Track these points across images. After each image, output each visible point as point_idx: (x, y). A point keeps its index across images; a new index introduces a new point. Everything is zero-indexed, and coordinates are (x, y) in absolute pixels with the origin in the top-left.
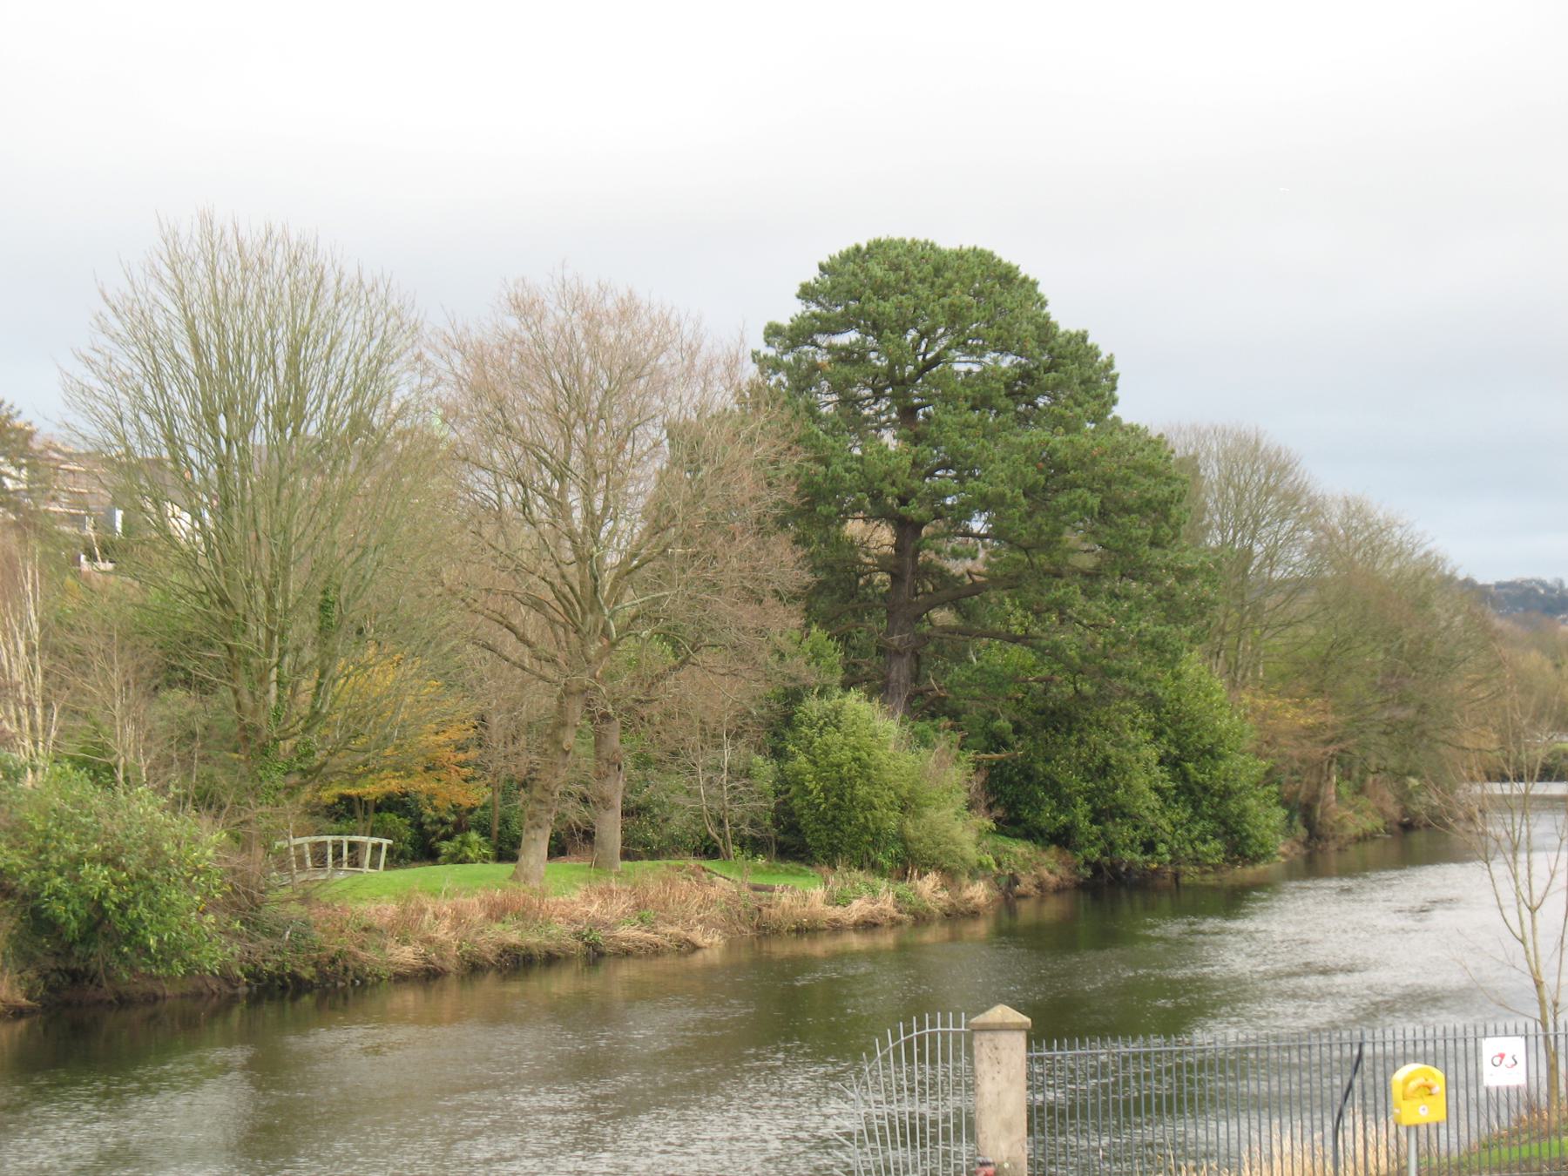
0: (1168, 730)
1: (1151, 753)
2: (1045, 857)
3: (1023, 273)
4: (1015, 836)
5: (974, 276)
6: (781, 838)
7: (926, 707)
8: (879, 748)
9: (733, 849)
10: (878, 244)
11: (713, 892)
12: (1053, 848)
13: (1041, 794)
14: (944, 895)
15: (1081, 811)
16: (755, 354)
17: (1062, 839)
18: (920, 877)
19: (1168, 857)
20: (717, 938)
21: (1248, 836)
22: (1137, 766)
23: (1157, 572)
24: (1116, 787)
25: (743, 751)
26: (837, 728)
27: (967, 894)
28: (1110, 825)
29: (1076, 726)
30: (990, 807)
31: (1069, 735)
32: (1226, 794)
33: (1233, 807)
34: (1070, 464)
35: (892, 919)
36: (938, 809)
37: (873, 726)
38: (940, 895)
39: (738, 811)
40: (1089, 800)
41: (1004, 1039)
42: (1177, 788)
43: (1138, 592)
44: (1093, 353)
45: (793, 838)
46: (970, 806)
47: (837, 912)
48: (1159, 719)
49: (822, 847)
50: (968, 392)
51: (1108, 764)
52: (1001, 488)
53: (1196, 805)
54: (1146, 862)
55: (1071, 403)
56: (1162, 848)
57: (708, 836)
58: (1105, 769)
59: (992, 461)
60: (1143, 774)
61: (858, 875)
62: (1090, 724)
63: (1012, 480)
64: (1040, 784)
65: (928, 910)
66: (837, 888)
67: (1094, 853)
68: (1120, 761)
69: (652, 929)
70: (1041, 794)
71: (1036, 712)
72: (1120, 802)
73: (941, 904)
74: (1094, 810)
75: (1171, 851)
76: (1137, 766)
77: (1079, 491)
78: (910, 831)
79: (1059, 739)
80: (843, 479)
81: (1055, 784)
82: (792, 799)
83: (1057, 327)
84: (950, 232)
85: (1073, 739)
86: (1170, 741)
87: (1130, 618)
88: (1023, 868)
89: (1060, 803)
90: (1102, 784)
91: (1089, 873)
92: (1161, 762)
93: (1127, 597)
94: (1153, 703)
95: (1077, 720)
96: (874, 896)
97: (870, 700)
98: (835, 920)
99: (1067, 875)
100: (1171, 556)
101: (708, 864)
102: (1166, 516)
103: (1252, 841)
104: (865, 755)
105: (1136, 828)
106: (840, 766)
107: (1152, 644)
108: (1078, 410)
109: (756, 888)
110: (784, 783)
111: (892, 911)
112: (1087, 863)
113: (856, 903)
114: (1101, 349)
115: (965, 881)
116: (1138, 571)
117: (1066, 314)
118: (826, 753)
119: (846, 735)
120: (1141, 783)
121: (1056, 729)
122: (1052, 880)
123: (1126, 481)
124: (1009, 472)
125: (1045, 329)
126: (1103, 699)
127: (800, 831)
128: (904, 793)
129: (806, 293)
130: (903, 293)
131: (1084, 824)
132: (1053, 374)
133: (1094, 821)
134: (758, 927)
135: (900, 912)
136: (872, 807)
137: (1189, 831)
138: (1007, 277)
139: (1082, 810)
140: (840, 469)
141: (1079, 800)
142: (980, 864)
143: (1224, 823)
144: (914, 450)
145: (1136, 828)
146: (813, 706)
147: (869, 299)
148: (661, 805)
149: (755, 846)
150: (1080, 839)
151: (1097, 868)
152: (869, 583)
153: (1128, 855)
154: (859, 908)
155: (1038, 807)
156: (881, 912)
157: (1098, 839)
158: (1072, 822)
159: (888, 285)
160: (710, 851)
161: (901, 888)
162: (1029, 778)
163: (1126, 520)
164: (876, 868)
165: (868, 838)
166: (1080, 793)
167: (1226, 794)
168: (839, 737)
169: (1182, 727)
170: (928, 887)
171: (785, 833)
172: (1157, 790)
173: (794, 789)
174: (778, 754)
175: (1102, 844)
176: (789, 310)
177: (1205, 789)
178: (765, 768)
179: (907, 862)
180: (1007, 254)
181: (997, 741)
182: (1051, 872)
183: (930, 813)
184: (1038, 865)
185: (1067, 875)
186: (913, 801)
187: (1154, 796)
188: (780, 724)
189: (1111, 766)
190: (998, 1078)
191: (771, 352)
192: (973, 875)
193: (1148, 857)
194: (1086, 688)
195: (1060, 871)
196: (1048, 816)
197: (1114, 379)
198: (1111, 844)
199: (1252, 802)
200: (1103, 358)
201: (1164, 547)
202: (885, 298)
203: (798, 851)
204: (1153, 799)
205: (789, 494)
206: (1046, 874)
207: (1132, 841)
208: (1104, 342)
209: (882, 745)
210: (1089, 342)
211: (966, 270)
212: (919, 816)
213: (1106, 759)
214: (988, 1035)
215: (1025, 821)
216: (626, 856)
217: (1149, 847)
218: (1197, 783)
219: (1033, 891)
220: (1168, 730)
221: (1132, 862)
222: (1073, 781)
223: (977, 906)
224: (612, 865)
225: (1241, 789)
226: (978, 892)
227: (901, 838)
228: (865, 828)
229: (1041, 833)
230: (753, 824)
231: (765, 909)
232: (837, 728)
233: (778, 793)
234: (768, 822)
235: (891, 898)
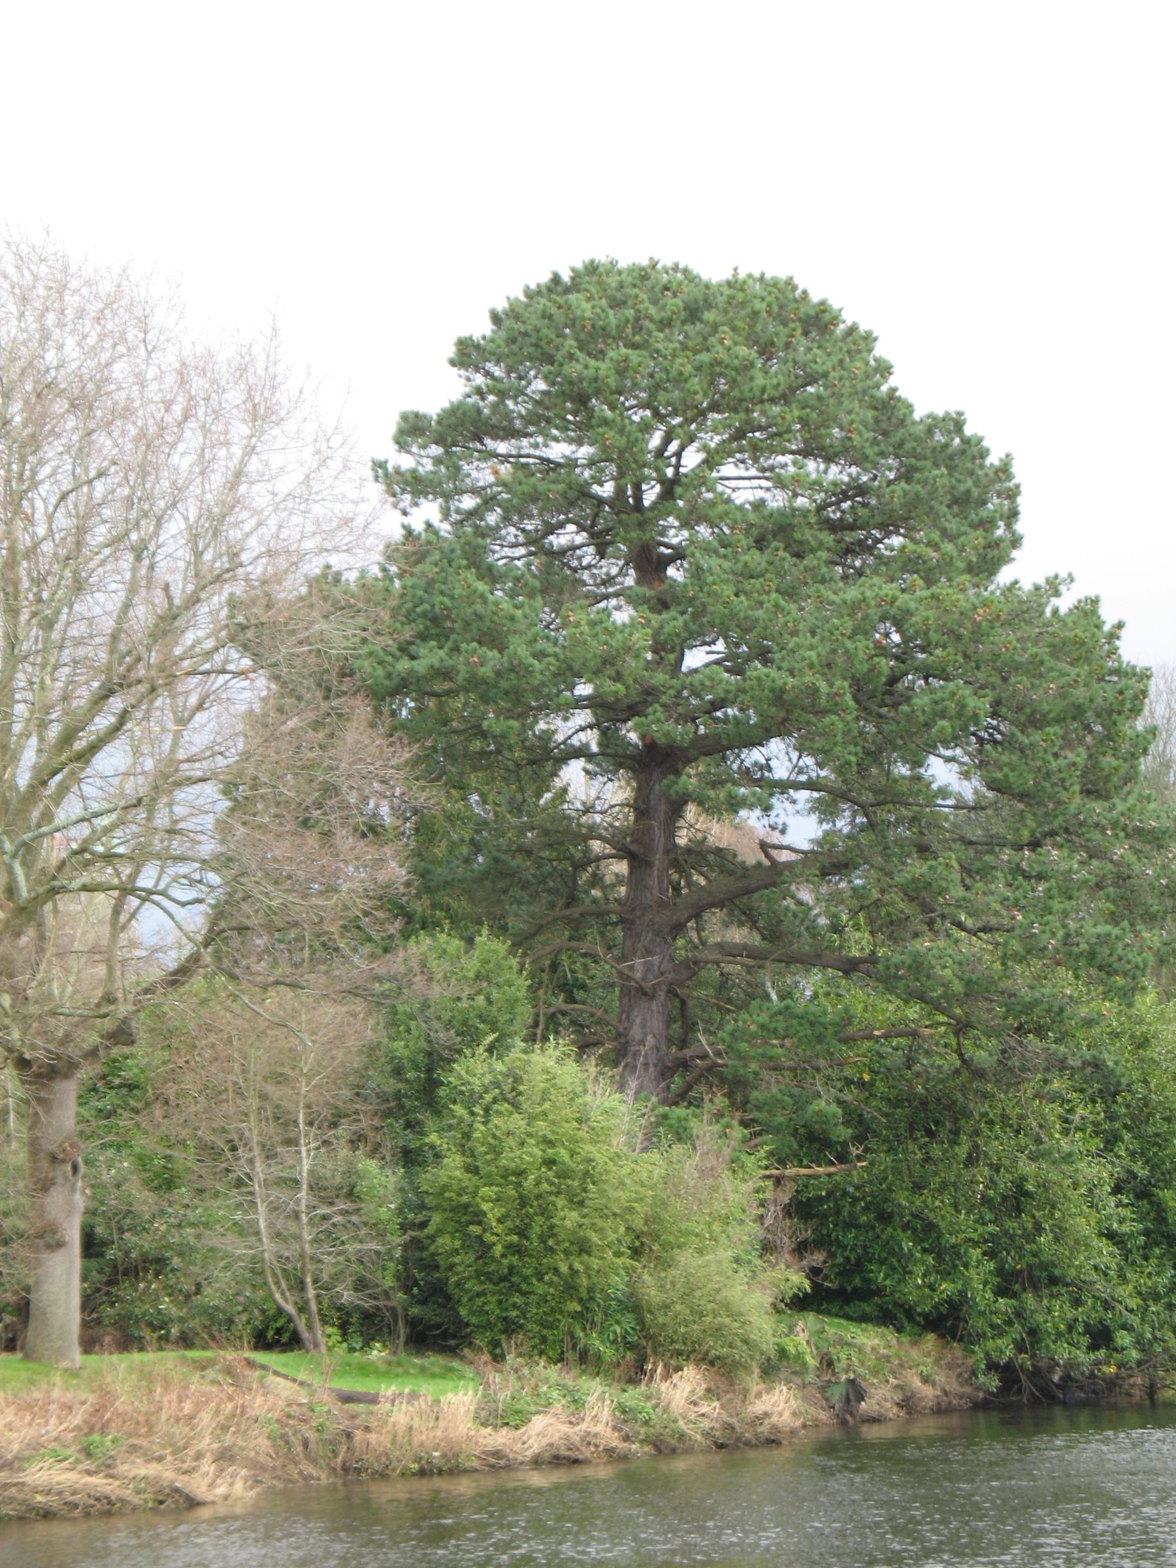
0: (1127, 1136)
1: (1099, 1172)
2: (914, 1353)
3: (849, 317)
4: (863, 1319)
5: (755, 314)
6: (415, 1311)
7: (682, 1078)
8: (594, 1142)
9: (325, 1335)
10: (592, 268)
11: (258, 1404)
12: (931, 1337)
13: (907, 1245)
14: (710, 1408)
15: (978, 1277)
16: (379, 465)
17: (947, 1323)
18: (667, 1376)
19: (1135, 1354)
20: (239, 1486)
22: (1073, 1195)
23: (1096, 836)
24: (1039, 1229)
25: (344, 1152)
26: (516, 1106)
27: (759, 1407)
28: (1029, 1299)
29: (966, 1126)
30: (801, 1249)
31: (954, 1142)
35: (610, 1451)
36: (700, 1251)
37: (579, 1108)
38: (705, 1409)
39: (329, 1264)
40: (990, 1254)
42: (1147, 1233)
43: (1064, 866)
44: (974, 450)
45: (429, 1316)
46: (767, 1248)
47: (499, 1439)
48: (1112, 1117)
49: (489, 1326)
52: (809, 678)
54: (1097, 1363)
55: (936, 536)
56: (1123, 1339)
57: (280, 1311)
58: (1018, 1199)
59: (794, 633)
61: (553, 1373)
62: (991, 1123)
64: (906, 1227)
65: (682, 1436)
66: (504, 1396)
67: (1004, 1348)
68: (1044, 1186)
69: (107, 1468)
70: (907, 1245)
71: (896, 1103)
72: (1045, 1258)
73: (706, 1424)
74: (1000, 1271)
75: (1139, 1343)
76: (1073, 1195)
78: (650, 1288)
79: (936, 1151)
80: (529, 672)
81: (930, 1227)
82: (432, 1238)
83: (910, 407)
84: (716, 253)
85: (962, 1151)
86: (1132, 1154)
88: (875, 1372)
89: (939, 1258)
90: (1012, 1225)
91: (993, 1383)
92: (1117, 1190)
93: (1040, 877)
94: (1104, 1086)
95: (968, 1115)
96: (561, 1412)
97: (579, 1059)
98: (497, 1454)
99: (954, 1387)
100: (1120, 806)
101: (260, 1357)
102: (1111, 736)
104: (564, 1155)
105: (1077, 1302)
106: (521, 1173)
107: (1091, 956)
108: (948, 547)
109: (348, 1398)
110: (415, 1212)
111: (613, 1440)
112: (992, 1366)
113: (539, 1423)
115: (754, 1382)
118: (496, 1151)
119: (531, 1119)
120: (1083, 1225)
121: (930, 1134)
122: (928, 1393)
123: (1035, 668)
124: (823, 650)
125: (890, 410)
126: (1008, 1073)
127: (448, 1298)
128: (638, 1223)
129: (467, 355)
130: (635, 346)
131: (982, 1296)
134: (346, 1469)
135: (626, 1438)
136: (583, 1248)
138: (819, 321)
140: (523, 652)
141: (975, 1253)
142: (782, 1353)
144: (656, 619)
145: (1077, 1302)
146: (474, 1070)
147: (571, 356)
148: (184, 1251)
149: (363, 1325)
151: (1008, 1373)
152: (596, 881)
153: (1063, 1353)
154: (544, 1430)
155: (901, 1267)
156: (588, 1439)
158: (963, 1293)
159: (605, 332)
160: (277, 1336)
161: (632, 1396)
162: (885, 1218)
163: (1037, 736)
164: (587, 1360)
165: (575, 1306)
166: (976, 1244)
168: (517, 1122)
169: (1151, 1130)
170: (681, 1393)
171: (423, 1302)
172: (1111, 1236)
173: (437, 1219)
174: (410, 1158)
175: (1017, 1331)
176: (444, 389)
178: (382, 1179)
179: (644, 1349)
180: (817, 287)
181: (814, 1142)
182: (926, 1380)
183: (685, 1258)
184: (897, 1370)
185: (954, 1387)
186: (655, 1237)
187: (1106, 1247)
188: (411, 1097)
189: (1027, 1194)
191: (406, 462)
192: (769, 1371)
193: (1101, 1354)
194: (983, 1056)
195: (940, 1378)
196: (919, 1285)
197: (1012, 494)
198: (1033, 1332)
200: (993, 459)
201: (1107, 798)
202: (600, 355)
203: (445, 1335)
204: (1106, 1254)
206: (917, 1383)
207: (1070, 1328)
208: (996, 434)
209: (599, 1136)
210: (968, 431)
211: (743, 304)
212: (665, 1264)
215: (880, 1292)
216: (89, 1344)
217: (1101, 1337)
219: (893, 1411)
220: (1127, 1136)
221: (1071, 1364)
222: (963, 1227)
223: (775, 1428)
224: (61, 1353)
226: (779, 1404)
227: (634, 1306)
228: (570, 1289)
229: (909, 1313)
230: (361, 1284)
231: (359, 1435)
232: (516, 1106)
233: (404, 1227)
234: (389, 1282)
235: (606, 1414)
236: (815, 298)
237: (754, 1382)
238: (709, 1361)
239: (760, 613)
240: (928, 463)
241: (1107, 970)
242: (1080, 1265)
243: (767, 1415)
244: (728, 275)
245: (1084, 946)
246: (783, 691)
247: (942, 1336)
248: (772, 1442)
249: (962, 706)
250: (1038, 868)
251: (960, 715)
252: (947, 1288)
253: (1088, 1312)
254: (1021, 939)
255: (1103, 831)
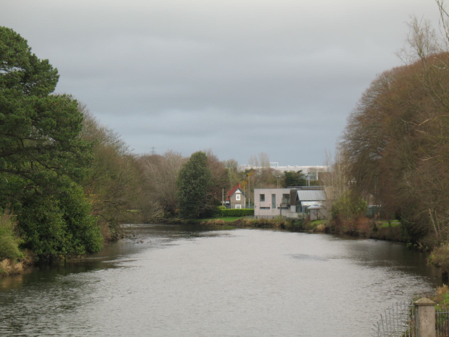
1: (61, 215)
5: (7, 37)
14: (10, 267)
21: (92, 244)
32: (85, 228)
33: (88, 234)
34: (46, 108)
41: (428, 308)
44: (49, 67)
50: (6, 81)
51: (45, 219)
53: (74, 233)
55: (43, 86)
56: (64, 249)
58: (43, 221)
59: (18, 107)
60: (58, 223)
63: (26, 113)
75: (67, 250)
77: (50, 119)
83: (37, 58)
87: (67, 165)
103: (93, 246)
107: (75, 174)
114: (53, 66)
116: (68, 149)
117: (40, 51)
125: (33, 59)
132: (37, 75)
133: (40, 240)
137: (72, 243)
138: (18, 39)
139: (37, 235)
143: (83, 239)
150: (35, 246)
157: (42, 246)
167: (85, 228)
177: (77, 227)
190: (427, 321)
192: (19, 261)
199: (93, 232)
205: (79, 126)
213: (45, 216)
214: (423, 307)
217: (59, 249)
218: (75, 225)
223: (19, 271)
225: (90, 227)
236: (17, 34)
237: (15, 261)
238: (8, 258)
239: (11, 102)
240: (42, 71)
241: (77, 176)
242: (58, 234)
243: (18, 268)
244: (51, 64)
245: (73, 172)
246: (17, 119)
247: (28, 249)
248: (19, 274)
249: (52, 123)
250: (64, 155)
251: (51, 124)
252: (30, 239)
253: (57, 244)
254: (62, 171)
255: (75, 147)
